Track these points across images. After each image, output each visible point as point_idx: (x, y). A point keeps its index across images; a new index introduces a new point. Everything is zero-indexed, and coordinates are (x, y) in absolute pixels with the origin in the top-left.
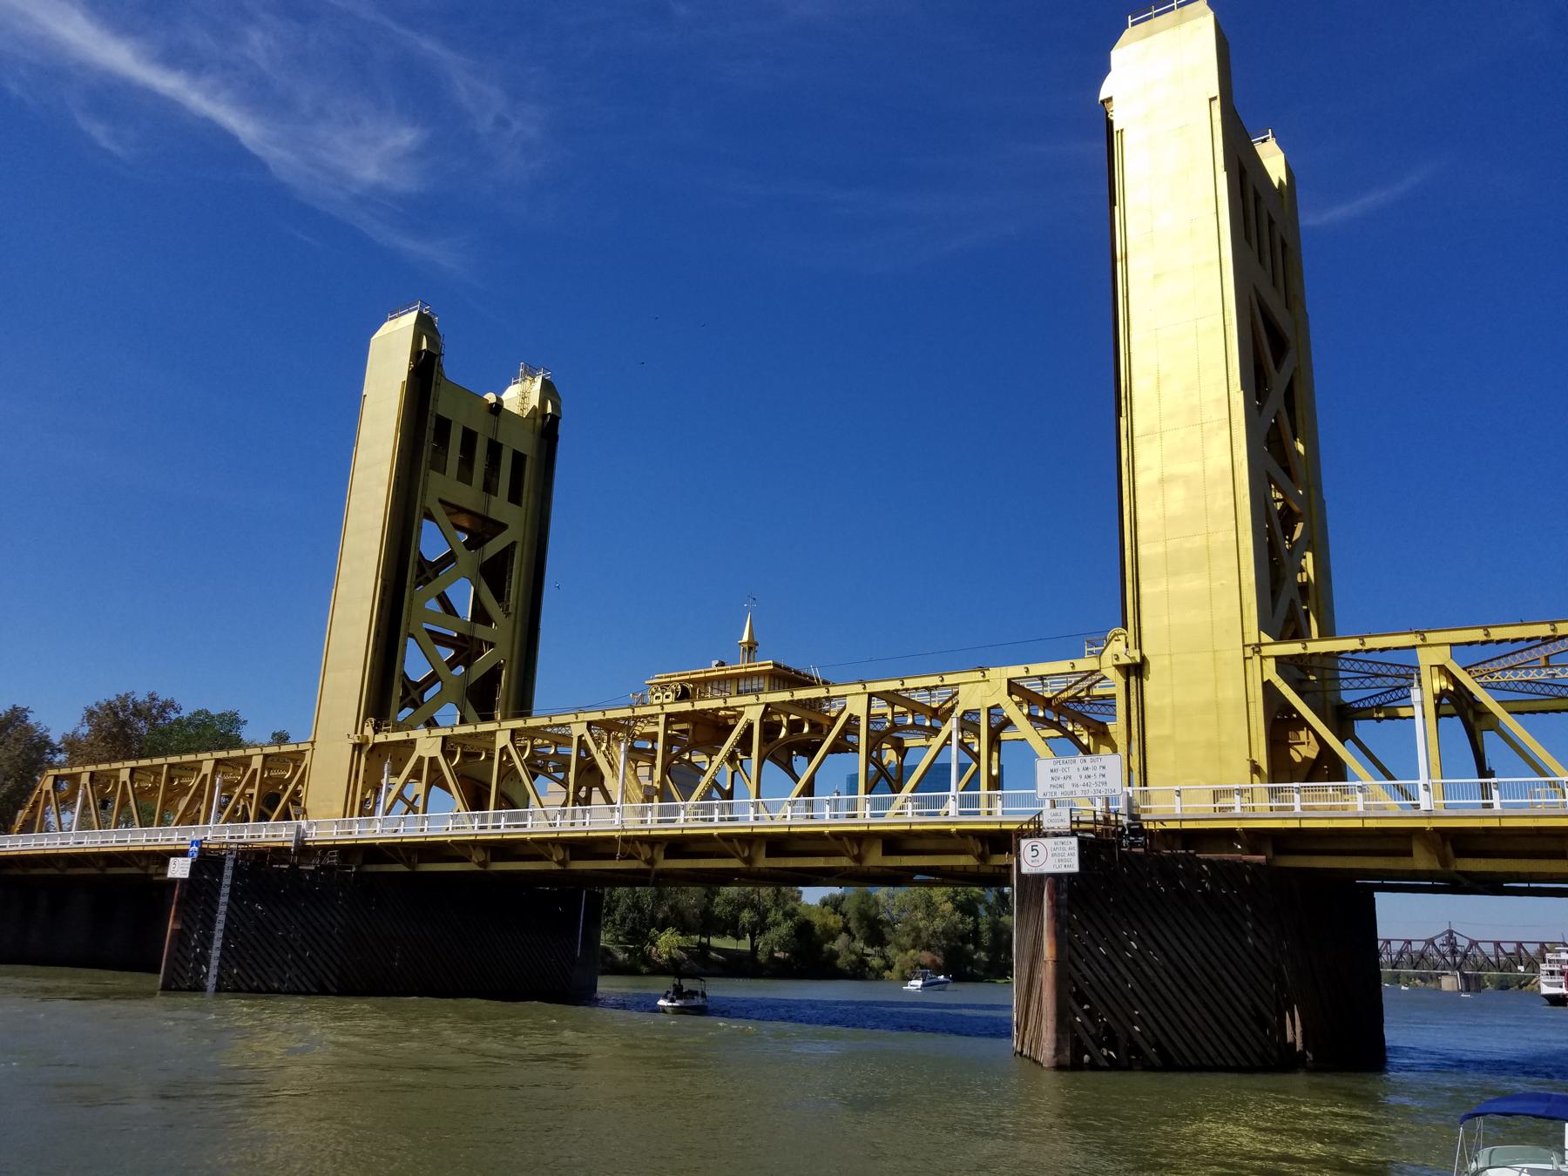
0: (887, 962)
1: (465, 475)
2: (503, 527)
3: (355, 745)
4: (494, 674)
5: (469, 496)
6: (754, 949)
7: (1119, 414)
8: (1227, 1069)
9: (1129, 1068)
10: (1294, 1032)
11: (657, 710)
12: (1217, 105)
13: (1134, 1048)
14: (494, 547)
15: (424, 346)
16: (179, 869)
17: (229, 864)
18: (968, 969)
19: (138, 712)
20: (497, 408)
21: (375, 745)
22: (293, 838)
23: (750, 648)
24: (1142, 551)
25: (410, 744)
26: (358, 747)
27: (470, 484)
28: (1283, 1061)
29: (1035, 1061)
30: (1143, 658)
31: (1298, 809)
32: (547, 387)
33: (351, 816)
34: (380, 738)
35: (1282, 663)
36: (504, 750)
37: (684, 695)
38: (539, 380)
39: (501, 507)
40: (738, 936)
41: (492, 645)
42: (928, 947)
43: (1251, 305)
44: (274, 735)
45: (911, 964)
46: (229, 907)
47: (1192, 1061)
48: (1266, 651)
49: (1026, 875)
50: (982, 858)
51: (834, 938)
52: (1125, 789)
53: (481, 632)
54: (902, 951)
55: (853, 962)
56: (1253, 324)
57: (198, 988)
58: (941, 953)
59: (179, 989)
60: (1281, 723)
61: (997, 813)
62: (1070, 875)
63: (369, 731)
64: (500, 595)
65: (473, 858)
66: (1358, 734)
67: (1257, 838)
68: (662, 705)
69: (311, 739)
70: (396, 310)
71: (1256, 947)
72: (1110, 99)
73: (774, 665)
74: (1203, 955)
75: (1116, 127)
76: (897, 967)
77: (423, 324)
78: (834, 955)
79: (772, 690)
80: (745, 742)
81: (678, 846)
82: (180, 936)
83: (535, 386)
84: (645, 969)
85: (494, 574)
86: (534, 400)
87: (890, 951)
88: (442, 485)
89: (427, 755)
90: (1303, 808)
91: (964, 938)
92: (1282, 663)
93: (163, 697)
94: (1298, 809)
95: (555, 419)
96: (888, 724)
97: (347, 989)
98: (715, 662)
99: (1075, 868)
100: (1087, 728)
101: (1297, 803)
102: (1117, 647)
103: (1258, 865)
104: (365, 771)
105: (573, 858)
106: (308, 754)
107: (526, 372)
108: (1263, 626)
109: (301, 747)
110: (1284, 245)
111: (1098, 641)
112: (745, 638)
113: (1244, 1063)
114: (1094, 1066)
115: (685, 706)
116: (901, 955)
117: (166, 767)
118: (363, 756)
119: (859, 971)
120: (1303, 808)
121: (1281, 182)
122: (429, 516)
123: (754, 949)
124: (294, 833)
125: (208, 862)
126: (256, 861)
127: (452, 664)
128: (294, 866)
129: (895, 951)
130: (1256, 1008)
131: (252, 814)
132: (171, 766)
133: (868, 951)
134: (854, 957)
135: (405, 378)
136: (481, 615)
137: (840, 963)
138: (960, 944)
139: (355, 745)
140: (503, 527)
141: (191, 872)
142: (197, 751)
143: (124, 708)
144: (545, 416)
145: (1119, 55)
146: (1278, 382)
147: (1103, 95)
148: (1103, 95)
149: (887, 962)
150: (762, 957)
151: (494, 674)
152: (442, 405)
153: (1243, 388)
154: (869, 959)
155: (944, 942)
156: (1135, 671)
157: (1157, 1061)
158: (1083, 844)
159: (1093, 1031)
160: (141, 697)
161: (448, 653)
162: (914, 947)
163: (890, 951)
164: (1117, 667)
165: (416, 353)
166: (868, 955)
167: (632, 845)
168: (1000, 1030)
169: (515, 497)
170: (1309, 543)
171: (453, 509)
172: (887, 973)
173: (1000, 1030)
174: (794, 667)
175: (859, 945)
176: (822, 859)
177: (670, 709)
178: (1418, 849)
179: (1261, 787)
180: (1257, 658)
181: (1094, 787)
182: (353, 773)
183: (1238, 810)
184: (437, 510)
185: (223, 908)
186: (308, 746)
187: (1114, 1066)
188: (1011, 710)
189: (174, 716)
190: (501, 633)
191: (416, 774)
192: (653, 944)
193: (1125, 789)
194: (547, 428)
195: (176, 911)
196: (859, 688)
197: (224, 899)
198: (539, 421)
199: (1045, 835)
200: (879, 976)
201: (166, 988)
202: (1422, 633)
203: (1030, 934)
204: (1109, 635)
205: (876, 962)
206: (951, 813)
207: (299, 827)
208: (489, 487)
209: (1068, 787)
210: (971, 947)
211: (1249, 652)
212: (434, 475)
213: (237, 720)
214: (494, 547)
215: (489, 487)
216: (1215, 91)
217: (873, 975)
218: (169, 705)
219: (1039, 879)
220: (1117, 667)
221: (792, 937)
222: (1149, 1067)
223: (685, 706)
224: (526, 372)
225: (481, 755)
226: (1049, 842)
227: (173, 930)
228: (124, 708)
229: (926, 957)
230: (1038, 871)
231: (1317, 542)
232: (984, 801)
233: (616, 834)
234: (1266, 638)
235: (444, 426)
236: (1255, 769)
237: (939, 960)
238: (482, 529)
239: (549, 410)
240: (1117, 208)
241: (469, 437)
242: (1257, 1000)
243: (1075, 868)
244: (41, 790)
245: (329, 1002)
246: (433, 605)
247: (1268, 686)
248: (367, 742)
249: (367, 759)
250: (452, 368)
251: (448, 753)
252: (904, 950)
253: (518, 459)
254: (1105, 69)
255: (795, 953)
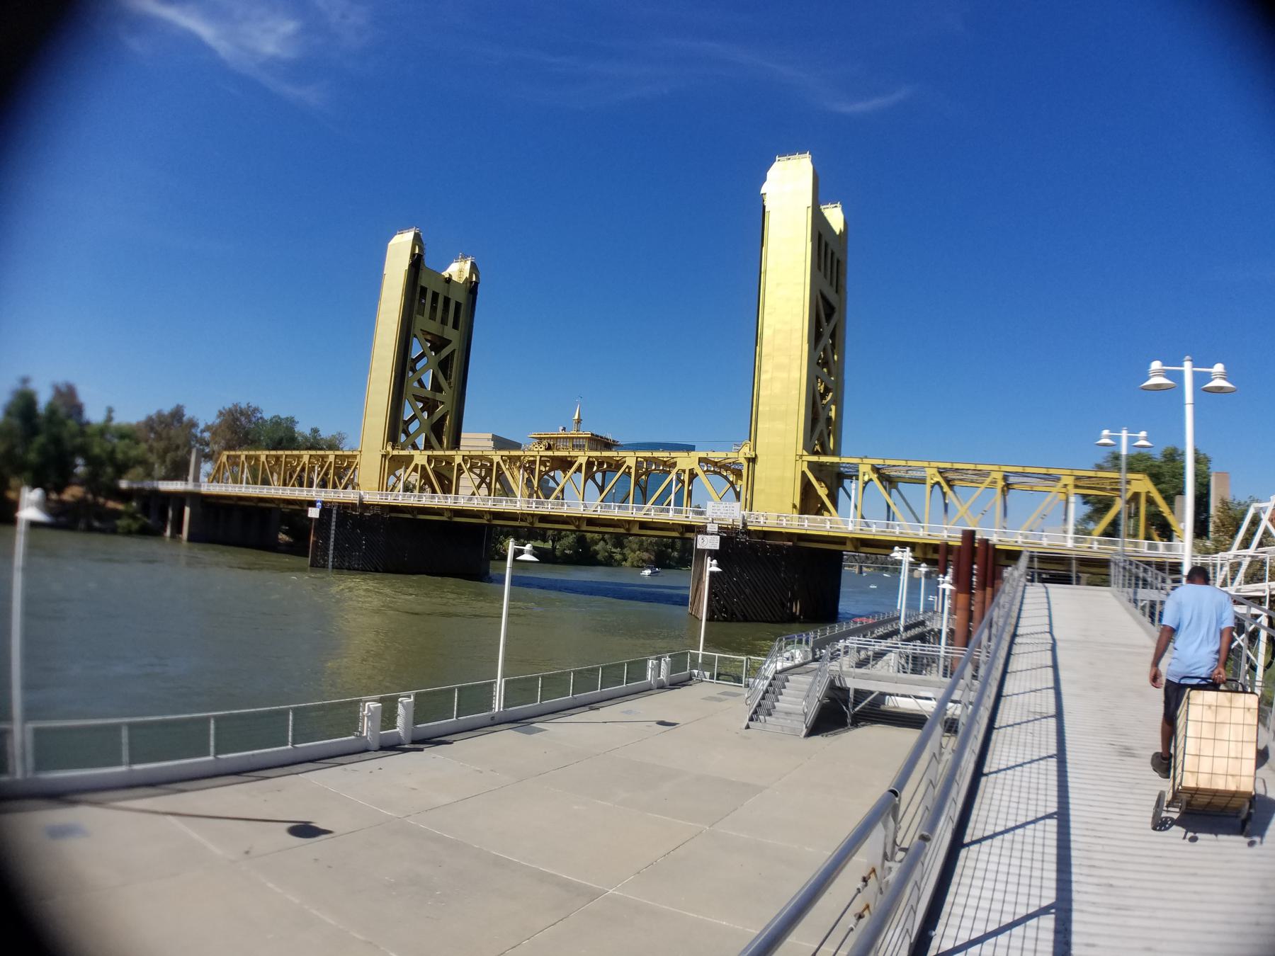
0: (624, 557)
1: (432, 317)
2: (449, 342)
3: (382, 455)
4: (443, 418)
5: (434, 327)
6: (554, 548)
7: (756, 345)
8: (767, 622)
9: (730, 621)
10: (796, 609)
11: (536, 453)
12: (810, 210)
13: (734, 613)
14: (445, 352)
15: (417, 251)
16: (314, 513)
17: (335, 512)
18: (668, 562)
19: (242, 413)
20: (449, 280)
21: (393, 456)
22: (358, 499)
23: (578, 422)
24: (760, 408)
25: (411, 458)
26: (384, 456)
27: (435, 320)
28: (792, 619)
29: (696, 617)
30: (756, 455)
31: (806, 526)
32: (473, 266)
33: (382, 491)
34: (395, 452)
35: (811, 465)
36: (459, 465)
37: (549, 448)
38: (469, 263)
39: (450, 333)
40: (545, 541)
41: (443, 403)
42: (647, 550)
43: (817, 299)
44: (312, 429)
45: (638, 559)
46: (335, 531)
47: (754, 618)
48: (804, 458)
49: (699, 549)
50: (682, 533)
51: (597, 544)
52: (742, 512)
53: (439, 397)
54: (632, 551)
55: (606, 557)
56: (817, 306)
57: (324, 566)
58: (654, 554)
59: (317, 567)
60: (807, 490)
61: (686, 516)
62: (715, 550)
63: (389, 449)
64: (447, 377)
65: (445, 514)
66: (845, 485)
67: (790, 536)
68: (538, 451)
69: (359, 450)
70: (402, 228)
71: (785, 578)
72: (765, 194)
73: (592, 434)
74: (763, 579)
75: (767, 210)
76: (629, 560)
77: (417, 239)
78: (596, 553)
79: (591, 449)
80: (579, 469)
81: (544, 518)
82: (315, 543)
83: (468, 266)
84: (497, 557)
85: (444, 366)
86: (466, 274)
87: (626, 551)
88: (423, 322)
89: (420, 463)
90: (808, 526)
91: (667, 546)
92: (811, 465)
93: (253, 405)
94: (806, 526)
95: (476, 283)
96: (644, 470)
97: (387, 570)
98: (562, 428)
99: (718, 548)
100: (733, 473)
101: (806, 523)
102: (746, 449)
103: (789, 546)
104: (389, 468)
105: (454, 516)
106: (358, 457)
107: (462, 258)
108: (805, 448)
109: (355, 453)
110: (838, 261)
111: (739, 446)
112: (576, 417)
113: (774, 620)
114: (718, 620)
115: (550, 453)
116: (632, 554)
117: (284, 456)
118: (387, 461)
119: (609, 562)
120: (808, 526)
121: (841, 231)
122: (415, 336)
123: (554, 548)
124: (358, 496)
125: (326, 509)
126: (344, 507)
127: (423, 410)
128: (361, 514)
129: (629, 551)
130: (781, 600)
131: (316, 481)
132: (286, 456)
133: (613, 550)
134: (607, 554)
135: (407, 268)
136: (437, 387)
137: (600, 557)
138: (664, 549)
139: (382, 455)
140: (449, 342)
141: (320, 515)
142: (257, 449)
143: (236, 411)
144: (471, 282)
145: (771, 174)
146: (827, 329)
147: (762, 192)
148: (762, 192)
149: (624, 557)
150: (558, 553)
151: (443, 418)
152: (424, 281)
153: (808, 342)
154: (614, 555)
155: (656, 548)
156: (752, 460)
157: (742, 619)
158: (722, 538)
159: (719, 607)
160: (244, 406)
161: (421, 405)
162: (639, 550)
163: (626, 551)
164: (745, 458)
165: (413, 255)
166: (614, 553)
167: (523, 517)
168: (683, 601)
169: (455, 326)
170: (834, 401)
171: (425, 332)
172: (624, 563)
173: (683, 601)
174: (600, 434)
175: (609, 547)
176: (612, 529)
177: (542, 454)
178: (848, 543)
179: (796, 515)
180: (800, 461)
181: (728, 514)
182: (382, 468)
183: (784, 524)
184: (419, 334)
185: (333, 532)
186: (358, 453)
187: (725, 620)
188: (698, 470)
189: (259, 415)
190: (446, 396)
191: (415, 469)
192: (501, 544)
193: (742, 512)
194: (472, 289)
195: (314, 532)
196: (632, 454)
197: (333, 528)
198: (468, 285)
199: (707, 534)
200: (619, 565)
201: (312, 565)
202: (862, 458)
203: (699, 569)
204: (743, 443)
205: (618, 557)
206: (671, 516)
207: (360, 494)
208: (444, 322)
209: (719, 514)
210: (670, 550)
211: (798, 458)
212: (419, 317)
213: (293, 421)
214: (445, 352)
215: (444, 322)
216: (810, 203)
217: (616, 564)
218: (256, 410)
219: (704, 551)
220: (745, 458)
221: (575, 543)
222: (738, 621)
223: (550, 453)
224: (462, 258)
225: (442, 462)
226: (709, 537)
227: (313, 541)
228: (236, 411)
229: (645, 556)
230: (704, 548)
231: (838, 401)
232: (630, 508)
233: (518, 512)
234: (805, 453)
235: (424, 290)
236: (794, 506)
237: (652, 557)
238: (438, 344)
239: (474, 279)
240: (764, 248)
241: (435, 295)
242: (782, 597)
243: (718, 548)
244: (221, 462)
245: (378, 575)
246: (416, 384)
247: (803, 473)
248: (389, 454)
249: (389, 462)
250: (428, 262)
251: (429, 462)
252: (634, 551)
253: (458, 305)
254: (764, 179)
255: (576, 552)
